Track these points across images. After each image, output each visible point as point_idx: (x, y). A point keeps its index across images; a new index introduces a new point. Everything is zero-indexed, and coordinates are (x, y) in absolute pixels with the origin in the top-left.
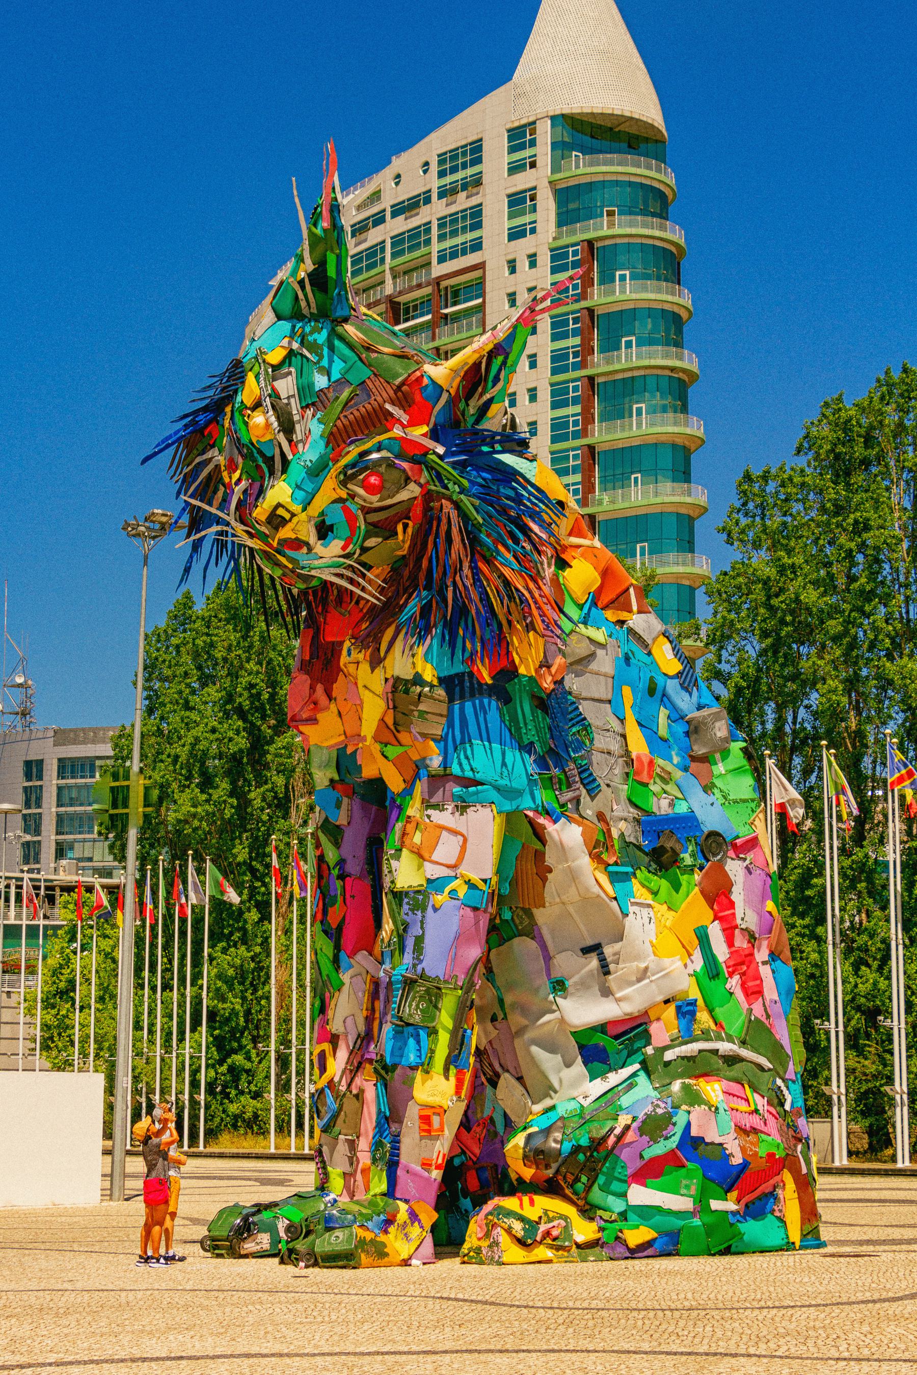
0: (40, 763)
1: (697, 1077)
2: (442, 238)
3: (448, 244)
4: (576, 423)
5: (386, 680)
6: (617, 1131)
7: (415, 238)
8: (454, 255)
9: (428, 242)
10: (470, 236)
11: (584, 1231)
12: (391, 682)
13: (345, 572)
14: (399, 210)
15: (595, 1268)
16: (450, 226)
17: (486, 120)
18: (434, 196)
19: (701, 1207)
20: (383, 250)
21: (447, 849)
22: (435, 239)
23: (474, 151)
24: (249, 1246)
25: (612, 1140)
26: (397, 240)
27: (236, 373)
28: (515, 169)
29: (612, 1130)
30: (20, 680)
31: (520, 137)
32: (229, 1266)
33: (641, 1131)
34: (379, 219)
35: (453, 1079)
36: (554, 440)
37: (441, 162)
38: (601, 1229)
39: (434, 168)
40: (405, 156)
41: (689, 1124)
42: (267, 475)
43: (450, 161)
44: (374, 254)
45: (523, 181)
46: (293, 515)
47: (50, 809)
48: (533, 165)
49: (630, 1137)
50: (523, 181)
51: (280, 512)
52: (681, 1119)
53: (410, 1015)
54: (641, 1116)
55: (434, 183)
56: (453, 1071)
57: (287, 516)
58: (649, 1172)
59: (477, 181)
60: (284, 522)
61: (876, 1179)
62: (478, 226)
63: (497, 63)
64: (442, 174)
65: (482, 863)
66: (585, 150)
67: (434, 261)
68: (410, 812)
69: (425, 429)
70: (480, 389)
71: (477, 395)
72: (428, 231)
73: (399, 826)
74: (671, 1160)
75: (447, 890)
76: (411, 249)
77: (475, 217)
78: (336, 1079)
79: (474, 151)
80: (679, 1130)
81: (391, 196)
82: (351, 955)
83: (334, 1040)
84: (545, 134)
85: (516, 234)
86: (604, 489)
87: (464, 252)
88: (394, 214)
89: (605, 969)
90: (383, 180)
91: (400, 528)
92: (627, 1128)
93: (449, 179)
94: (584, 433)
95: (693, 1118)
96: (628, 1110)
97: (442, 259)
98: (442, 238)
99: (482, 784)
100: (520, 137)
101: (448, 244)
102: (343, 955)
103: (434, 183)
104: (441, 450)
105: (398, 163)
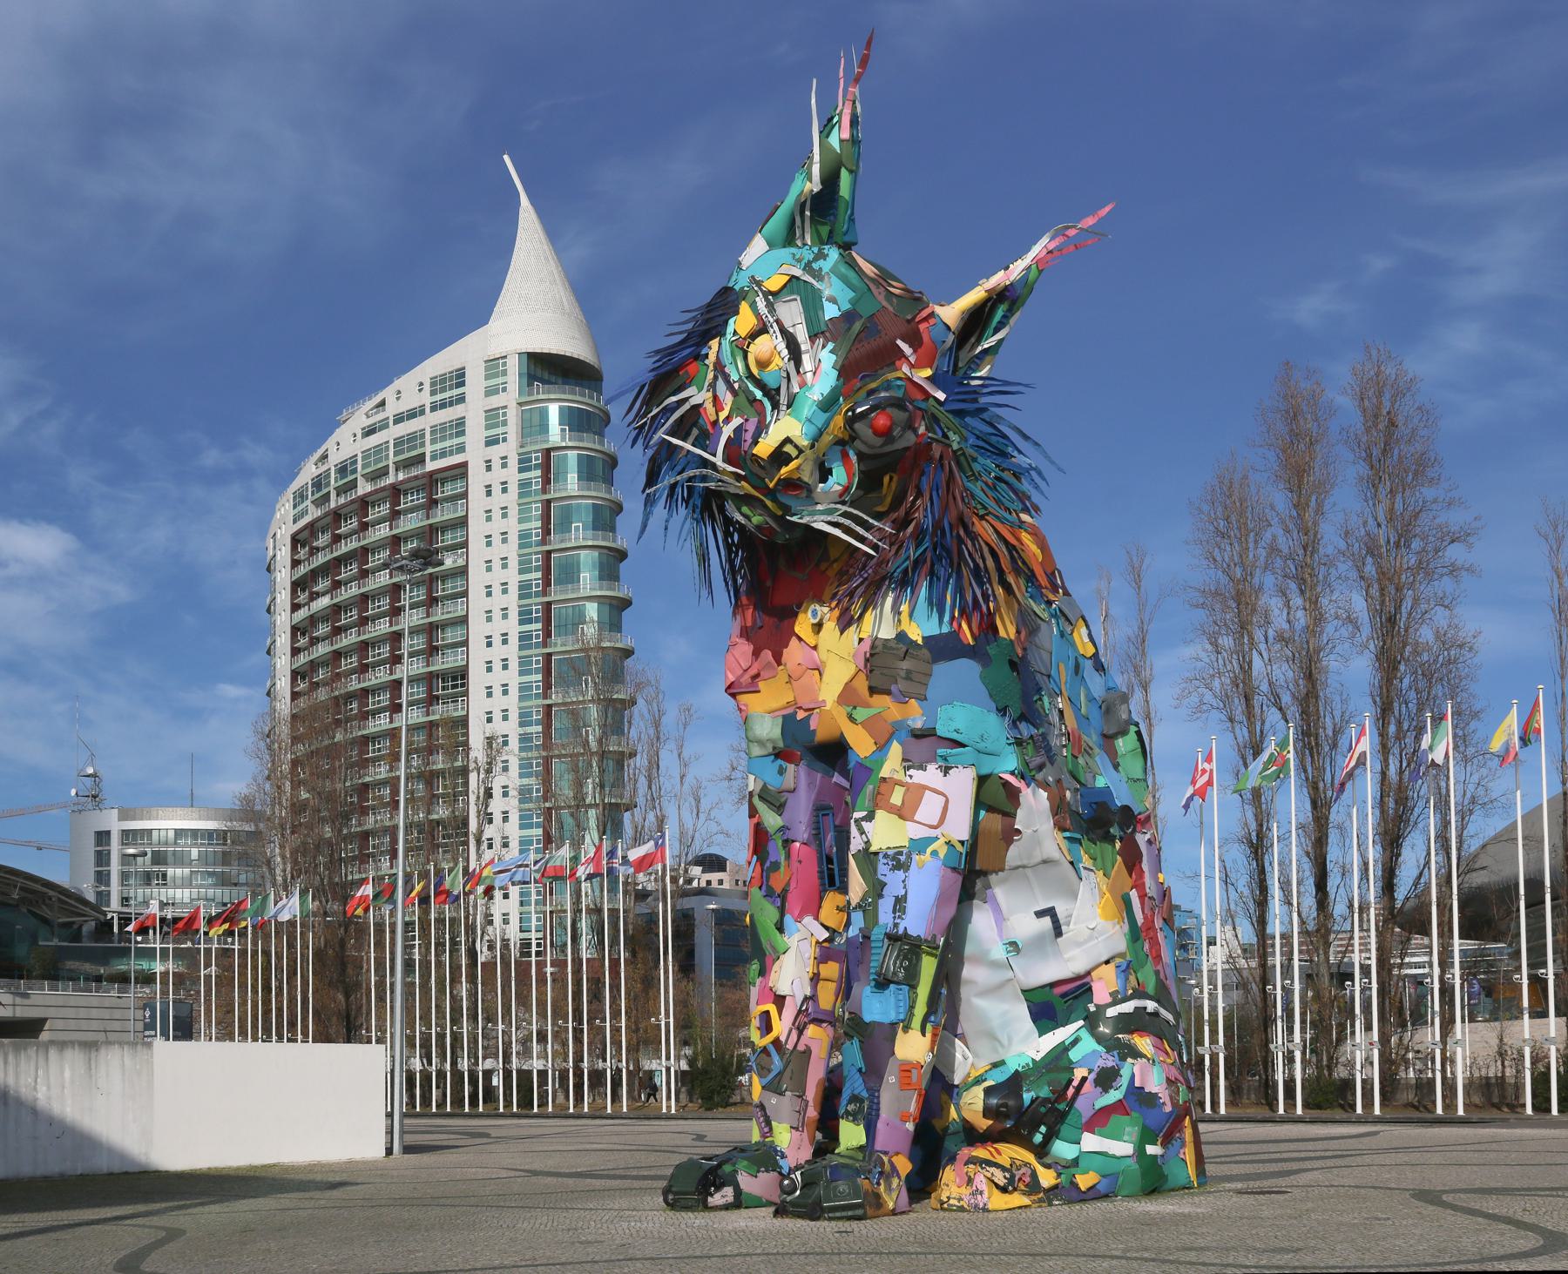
0: (108, 833)
1: (1131, 1032)
2: (433, 441)
3: (439, 446)
4: (537, 586)
5: (861, 640)
6: (1075, 1083)
7: (415, 438)
8: (443, 454)
9: (423, 445)
10: (456, 441)
11: (1047, 1178)
12: (866, 646)
13: (842, 520)
14: (399, 419)
15: (1060, 1211)
16: (440, 432)
17: (468, 352)
18: (428, 410)
19: (1140, 1151)
20: (387, 448)
21: (929, 809)
22: (428, 443)
23: (304, 488)
24: (717, 1199)
25: (1071, 1091)
26: (398, 442)
27: (725, 302)
28: (490, 392)
29: (1070, 1081)
30: (90, 771)
31: (494, 366)
32: (695, 1220)
33: (1097, 1082)
34: (383, 425)
35: (929, 1035)
36: (521, 597)
37: (433, 384)
38: (1059, 1175)
39: (427, 387)
40: (404, 378)
41: (1133, 1076)
42: (768, 407)
43: (439, 384)
44: (380, 451)
45: (496, 401)
46: (801, 451)
47: (115, 868)
48: (504, 390)
49: (1088, 1086)
50: (496, 401)
51: (788, 448)
52: (1125, 1073)
53: (894, 973)
54: (1096, 1070)
55: (427, 399)
56: (929, 1027)
57: (794, 453)
58: (1098, 1121)
59: (461, 399)
60: (788, 459)
61: (1239, 1125)
62: (462, 433)
63: (478, 314)
64: (433, 393)
65: (959, 828)
66: (544, 382)
67: (428, 459)
68: (885, 772)
69: (928, 372)
70: (973, 340)
71: (968, 346)
72: (423, 436)
73: (869, 788)
74: (1118, 1108)
75: (929, 850)
76: (410, 449)
77: (459, 426)
78: (783, 1039)
79: (459, 378)
80: (1124, 1082)
81: (392, 409)
82: (798, 919)
83: (780, 1001)
84: (514, 367)
85: (491, 442)
86: (559, 635)
87: (451, 453)
88: (396, 422)
89: (1058, 931)
90: (388, 393)
91: (886, 479)
92: (1084, 1079)
93: (439, 397)
94: (544, 593)
95: (1136, 1070)
96: (1080, 1064)
97: (434, 458)
98: (433, 441)
99: (964, 746)
100: (494, 366)
101: (439, 446)
102: (788, 919)
103: (427, 399)
104: (941, 396)
105: (398, 383)
